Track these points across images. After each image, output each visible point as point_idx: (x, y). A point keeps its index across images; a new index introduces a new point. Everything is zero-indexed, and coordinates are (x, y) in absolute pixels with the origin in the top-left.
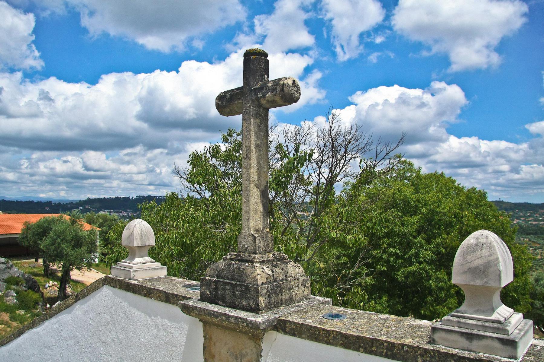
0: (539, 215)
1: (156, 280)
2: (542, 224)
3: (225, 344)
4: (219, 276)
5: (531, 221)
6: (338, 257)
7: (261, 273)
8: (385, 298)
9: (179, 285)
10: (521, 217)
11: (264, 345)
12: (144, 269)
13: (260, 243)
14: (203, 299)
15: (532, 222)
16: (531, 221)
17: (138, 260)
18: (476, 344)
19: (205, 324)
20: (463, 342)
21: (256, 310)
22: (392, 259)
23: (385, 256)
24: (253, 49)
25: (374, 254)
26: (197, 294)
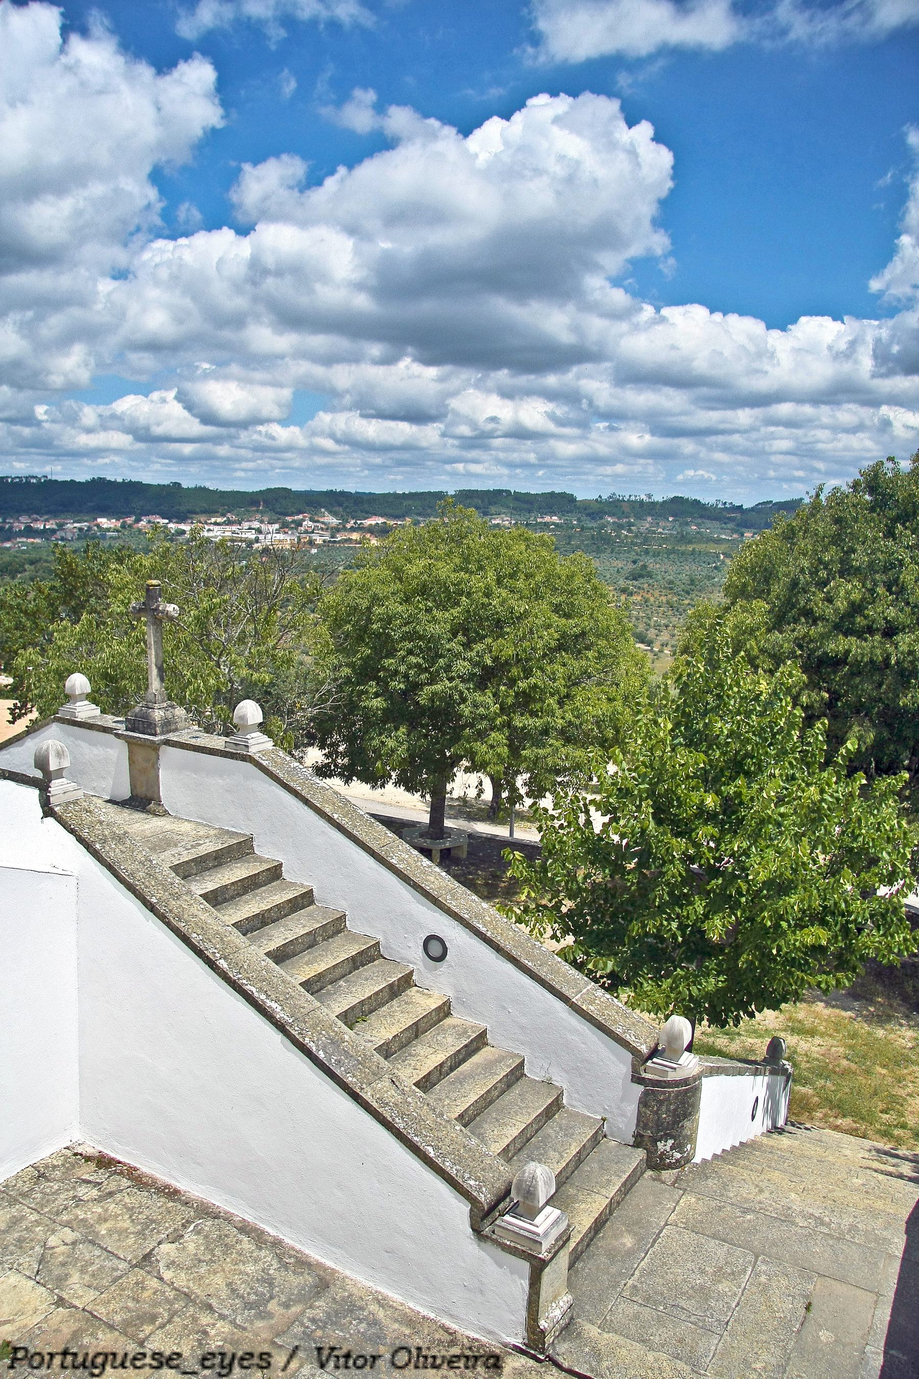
1: (93, 717)
3: (141, 754)
4: (136, 716)
6: (335, 668)
7: (158, 715)
8: (403, 730)
9: (109, 720)
11: (160, 753)
12: (86, 711)
13: (159, 698)
14: (126, 730)
17: (78, 704)
19: (129, 743)
21: (155, 735)
22: (412, 672)
23: (402, 669)
25: (386, 665)
26: (123, 726)
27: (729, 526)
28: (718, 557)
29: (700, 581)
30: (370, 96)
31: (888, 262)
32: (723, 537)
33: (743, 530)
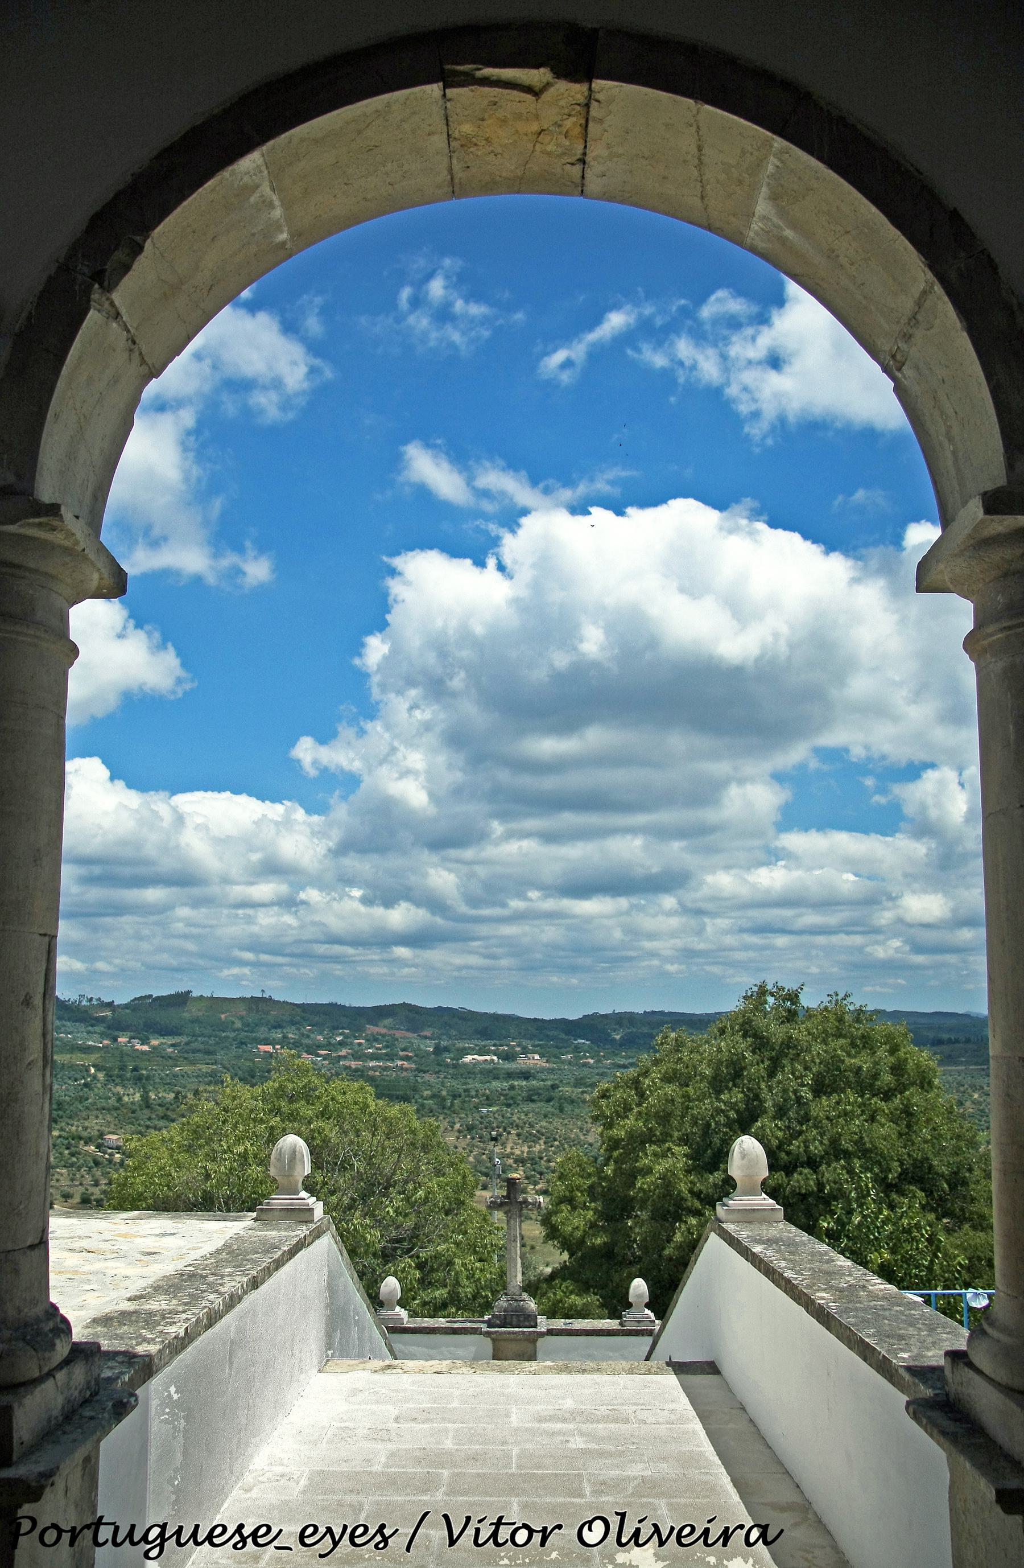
0: (367, 1040)
2: (372, 1068)
5: (345, 1057)
10: (320, 1047)
15: (347, 1063)
16: (345, 1057)
18: (641, 1324)
20: (636, 1324)
24: (567, 1370)
27: (97, 1029)
28: (88, 1070)
29: (70, 1104)
30: (756, 504)
31: (448, 552)
32: (90, 1043)
33: (116, 1033)
